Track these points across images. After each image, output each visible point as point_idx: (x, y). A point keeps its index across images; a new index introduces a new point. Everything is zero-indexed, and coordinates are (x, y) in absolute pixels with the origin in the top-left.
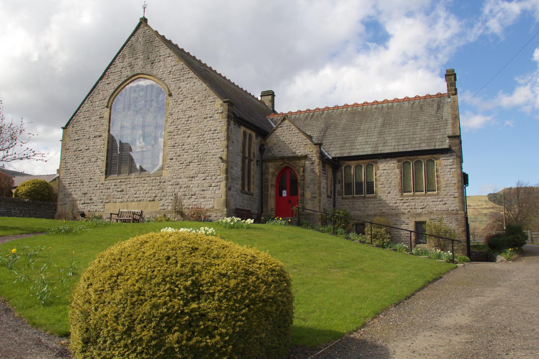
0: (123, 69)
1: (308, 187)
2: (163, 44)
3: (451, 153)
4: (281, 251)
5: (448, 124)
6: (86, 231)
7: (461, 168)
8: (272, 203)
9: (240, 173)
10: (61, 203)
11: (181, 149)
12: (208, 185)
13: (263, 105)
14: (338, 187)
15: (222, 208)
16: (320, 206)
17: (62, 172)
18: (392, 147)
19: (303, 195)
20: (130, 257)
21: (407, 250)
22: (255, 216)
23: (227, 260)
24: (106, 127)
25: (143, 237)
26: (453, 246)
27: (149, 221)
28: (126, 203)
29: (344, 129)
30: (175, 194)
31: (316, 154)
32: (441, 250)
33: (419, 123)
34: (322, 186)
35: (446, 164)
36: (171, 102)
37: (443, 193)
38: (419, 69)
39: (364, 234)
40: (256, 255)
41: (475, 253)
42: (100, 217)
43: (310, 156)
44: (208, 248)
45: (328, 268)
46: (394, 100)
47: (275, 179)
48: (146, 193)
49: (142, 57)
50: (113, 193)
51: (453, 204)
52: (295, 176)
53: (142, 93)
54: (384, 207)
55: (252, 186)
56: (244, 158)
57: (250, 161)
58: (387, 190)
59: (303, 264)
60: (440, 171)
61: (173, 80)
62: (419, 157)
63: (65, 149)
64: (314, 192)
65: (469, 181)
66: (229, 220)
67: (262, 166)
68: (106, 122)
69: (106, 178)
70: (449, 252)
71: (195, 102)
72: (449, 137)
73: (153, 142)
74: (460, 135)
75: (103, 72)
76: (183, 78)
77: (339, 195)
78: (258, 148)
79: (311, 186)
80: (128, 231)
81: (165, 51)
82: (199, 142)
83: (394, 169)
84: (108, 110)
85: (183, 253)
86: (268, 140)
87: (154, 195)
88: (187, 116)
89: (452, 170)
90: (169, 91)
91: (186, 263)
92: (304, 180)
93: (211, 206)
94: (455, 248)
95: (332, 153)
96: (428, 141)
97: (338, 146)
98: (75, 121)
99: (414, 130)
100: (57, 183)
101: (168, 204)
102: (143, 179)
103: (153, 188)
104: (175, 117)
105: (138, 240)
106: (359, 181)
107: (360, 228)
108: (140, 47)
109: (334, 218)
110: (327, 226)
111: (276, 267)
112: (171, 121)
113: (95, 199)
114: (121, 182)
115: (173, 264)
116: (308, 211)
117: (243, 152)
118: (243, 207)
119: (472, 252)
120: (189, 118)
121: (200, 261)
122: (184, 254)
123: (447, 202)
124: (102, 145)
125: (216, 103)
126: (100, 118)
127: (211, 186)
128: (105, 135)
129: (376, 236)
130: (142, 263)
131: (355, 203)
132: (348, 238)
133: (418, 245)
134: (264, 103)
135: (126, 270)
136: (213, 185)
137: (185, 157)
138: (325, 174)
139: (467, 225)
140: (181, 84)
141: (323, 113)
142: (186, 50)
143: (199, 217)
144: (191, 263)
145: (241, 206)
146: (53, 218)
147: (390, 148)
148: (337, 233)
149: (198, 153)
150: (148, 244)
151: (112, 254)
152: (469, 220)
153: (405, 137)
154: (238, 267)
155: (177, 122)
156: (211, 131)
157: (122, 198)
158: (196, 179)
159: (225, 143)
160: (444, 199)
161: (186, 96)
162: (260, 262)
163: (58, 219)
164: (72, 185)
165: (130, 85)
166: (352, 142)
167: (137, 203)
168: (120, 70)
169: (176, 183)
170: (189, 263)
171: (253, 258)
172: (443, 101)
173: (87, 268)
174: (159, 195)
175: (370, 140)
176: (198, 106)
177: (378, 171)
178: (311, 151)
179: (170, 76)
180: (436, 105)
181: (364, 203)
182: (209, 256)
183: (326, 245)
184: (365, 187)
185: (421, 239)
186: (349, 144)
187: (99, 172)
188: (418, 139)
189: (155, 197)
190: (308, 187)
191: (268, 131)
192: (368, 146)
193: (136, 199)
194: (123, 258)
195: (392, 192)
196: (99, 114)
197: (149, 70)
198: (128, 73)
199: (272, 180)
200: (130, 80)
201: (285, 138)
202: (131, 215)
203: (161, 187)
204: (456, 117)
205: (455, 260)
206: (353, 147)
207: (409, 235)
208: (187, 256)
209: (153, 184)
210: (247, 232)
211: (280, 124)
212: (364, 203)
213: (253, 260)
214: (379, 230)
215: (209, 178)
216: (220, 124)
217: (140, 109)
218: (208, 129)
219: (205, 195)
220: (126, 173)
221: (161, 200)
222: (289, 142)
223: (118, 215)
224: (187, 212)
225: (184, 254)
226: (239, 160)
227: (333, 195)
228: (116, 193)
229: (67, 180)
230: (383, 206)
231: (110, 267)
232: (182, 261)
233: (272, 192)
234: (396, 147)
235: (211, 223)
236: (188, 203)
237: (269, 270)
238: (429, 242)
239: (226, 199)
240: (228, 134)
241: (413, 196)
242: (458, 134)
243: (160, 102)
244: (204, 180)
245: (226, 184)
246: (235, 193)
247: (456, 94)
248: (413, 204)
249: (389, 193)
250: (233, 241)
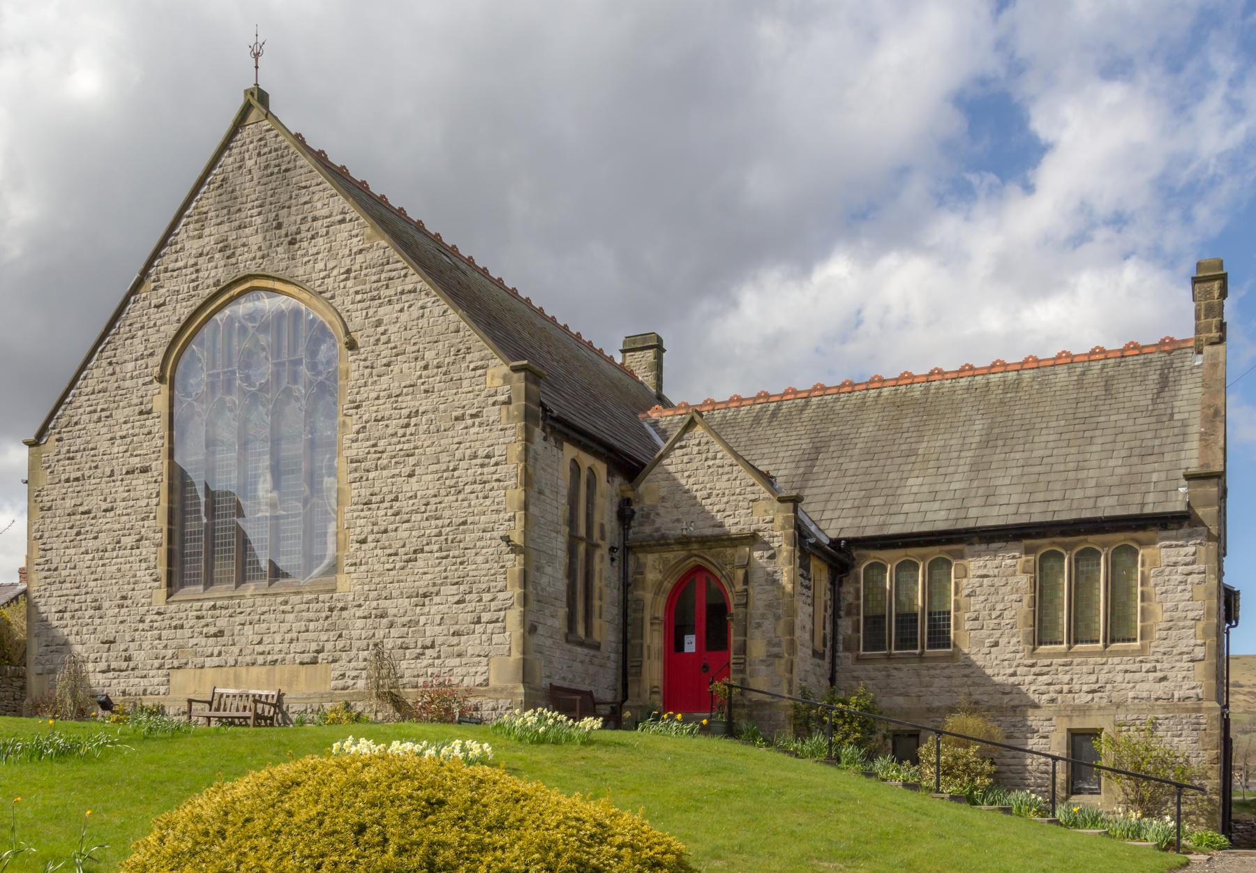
0: (201, 260)
1: (759, 625)
2: (321, 178)
3: (1190, 526)
4: (678, 808)
5: (1189, 438)
6: (119, 752)
7: (1220, 572)
8: (653, 672)
9: (562, 586)
10: (39, 669)
11: (390, 512)
12: (470, 617)
13: (629, 380)
14: (846, 625)
15: (510, 685)
16: (790, 682)
17: (34, 576)
18: (1012, 509)
19: (743, 649)
20: (249, 825)
21: (1042, 812)
22: (606, 710)
23: (527, 834)
24: (160, 442)
25: (286, 770)
26: (1179, 804)
27: (302, 723)
28: (232, 670)
29: (869, 454)
30: (376, 645)
31: (783, 528)
32: (1144, 815)
33: (1098, 433)
34: (798, 622)
35: (1173, 559)
36: (354, 366)
37: (1157, 646)
38: (1126, 257)
39: (916, 761)
40: (608, 822)
41: (1246, 823)
42: (160, 711)
43: (765, 535)
44: (473, 802)
45: (810, 858)
46: (1026, 361)
47: (662, 601)
48: (291, 641)
49: (259, 220)
50: (194, 641)
51: (1190, 680)
52: (721, 593)
53: (264, 339)
54: (978, 685)
55: (596, 622)
57: (592, 547)
58: (989, 636)
59: (741, 846)
60: (1152, 581)
61: (359, 297)
62: (1091, 538)
63: (38, 507)
65: (1241, 613)
66: (530, 718)
68: (159, 426)
69: (169, 596)
70: (1168, 818)
71: (426, 367)
72: (1189, 477)
73: (305, 489)
74: (1224, 472)
75: (141, 266)
76: (388, 292)
77: (846, 649)
78: (615, 509)
79: (768, 624)
80: (242, 749)
81: (329, 202)
82: (443, 492)
83: (1014, 574)
84: (165, 388)
85: (401, 815)
86: (642, 487)
87: (314, 646)
88: (405, 412)
89: (1190, 579)
90: (347, 333)
91: (412, 844)
92: (746, 605)
93: (479, 679)
94: (1184, 808)
95: (834, 524)
96: (1124, 489)
97: (849, 504)
98: (63, 421)
99: (1080, 457)
100: (24, 611)
101: (355, 673)
102: (280, 599)
103: (312, 626)
104: (367, 413)
105: (272, 777)
106: (907, 610)
107: (905, 746)
108: (250, 188)
109: (830, 716)
110: (811, 738)
111: (664, 853)
112: (356, 428)
113: (139, 657)
114: (214, 607)
115: (373, 846)
116: (756, 697)
117: (572, 522)
118: (571, 681)
119: (1237, 822)
120: (409, 416)
121: (452, 836)
122: (404, 817)
123: (1169, 674)
124: (150, 494)
125: (490, 372)
126: (141, 413)
127: (479, 622)
128: (160, 466)
129: (951, 768)
130: (285, 843)
131: (895, 673)
132: (869, 774)
133: (1074, 799)
134: (631, 374)
135: (239, 862)
136: (485, 617)
137: (402, 534)
138: (808, 588)
139: (1227, 742)
140: (382, 311)
141: (807, 404)
142: (395, 203)
143: (448, 710)
144: (426, 842)
145: (564, 679)
146: (17, 712)
147: (1004, 510)
148: (838, 760)
149: (440, 523)
150: (301, 791)
151: (198, 819)
152: (1232, 727)
153: (1052, 477)
154: (558, 855)
155: (376, 430)
156: (475, 457)
157: (220, 654)
158: (437, 599)
159: (518, 494)
160: (1159, 666)
161: (400, 349)
162: (618, 840)
163: (31, 716)
164: (67, 615)
165: (227, 312)
166: (890, 492)
167: (264, 669)
168: (192, 261)
169: (379, 612)
170: (419, 844)
171: (599, 830)
172: (1177, 364)
173: (125, 856)
174: (329, 646)
175: (945, 487)
176: (436, 382)
177: (965, 581)
178: (770, 520)
179: (349, 283)
180: (1154, 376)
181: (919, 675)
182: (476, 824)
183: (808, 792)
184: (923, 629)
185: (1085, 780)
186: (880, 501)
187: (148, 578)
188: (1092, 483)
189: (318, 652)
190: (759, 625)
191: (643, 459)
192: (936, 505)
193: (260, 659)
194: (230, 829)
195: (1003, 641)
196: (135, 401)
197: (283, 264)
198: (215, 272)
199: (653, 605)
200: (226, 296)
201: (692, 480)
202: (250, 703)
203: (334, 624)
204: (1216, 413)
205: (1183, 842)
206: (894, 509)
207: (1050, 769)
208: (414, 822)
209: (311, 615)
210: (581, 754)
211: (679, 438)
212: (919, 675)
213: (601, 834)
214: (961, 751)
215: (474, 596)
216: (503, 437)
217: (264, 388)
218: (468, 452)
219: (462, 648)
220: (229, 580)
221: (334, 661)
222: (705, 493)
223: (210, 703)
224: (410, 696)
225: (404, 817)
226: (559, 544)
227: (830, 650)
228: (203, 641)
229: (53, 600)
230: (974, 684)
231: (193, 854)
232: (401, 837)
233: (654, 640)
234: (1022, 509)
235: (481, 727)
236: (413, 672)
237: (643, 864)
238: (1109, 790)
239: (524, 660)
240: (526, 469)
241: (1066, 655)
242: (1218, 468)
243: (320, 367)
244: (458, 602)
245: (524, 615)
246: (549, 642)
247: (1222, 340)
248: (1066, 678)
249: (996, 644)
250: (544, 778)
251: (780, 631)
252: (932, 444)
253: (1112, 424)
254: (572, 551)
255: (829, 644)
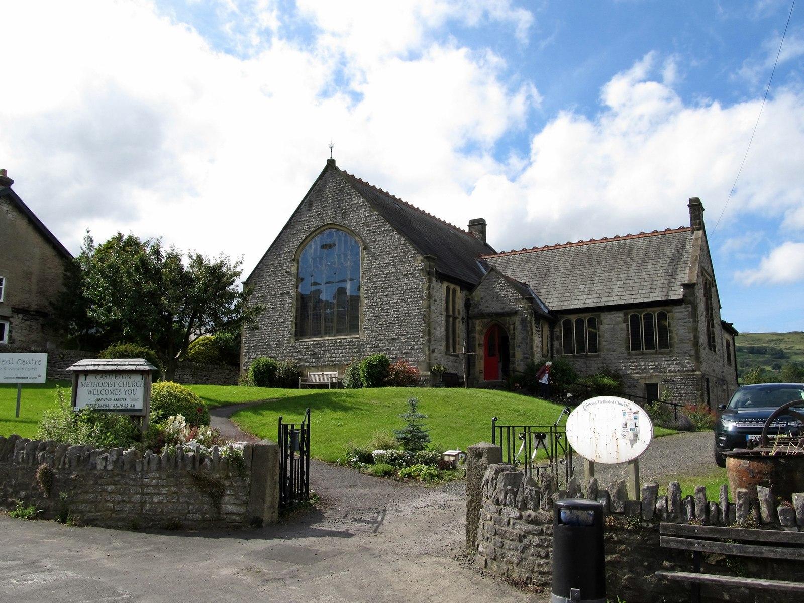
9: (444, 334)
11: (380, 309)
14: (556, 344)
19: (514, 355)
34: (535, 345)
37: (675, 350)
47: (483, 337)
56: (448, 316)
57: (455, 318)
62: (649, 309)
64: (526, 352)
67: (468, 323)
78: (464, 302)
86: (474, 294)
117: (447, 309)
136: (416, 347)
177: (602, 326)
181: (586, 363)
186: (569, 295)
193: (331, 364)
212: (586, 363)
251: (528, 348)
252: (590, 271)
253: (649, 270)
254: (447, 321)
255: (550, 352)
